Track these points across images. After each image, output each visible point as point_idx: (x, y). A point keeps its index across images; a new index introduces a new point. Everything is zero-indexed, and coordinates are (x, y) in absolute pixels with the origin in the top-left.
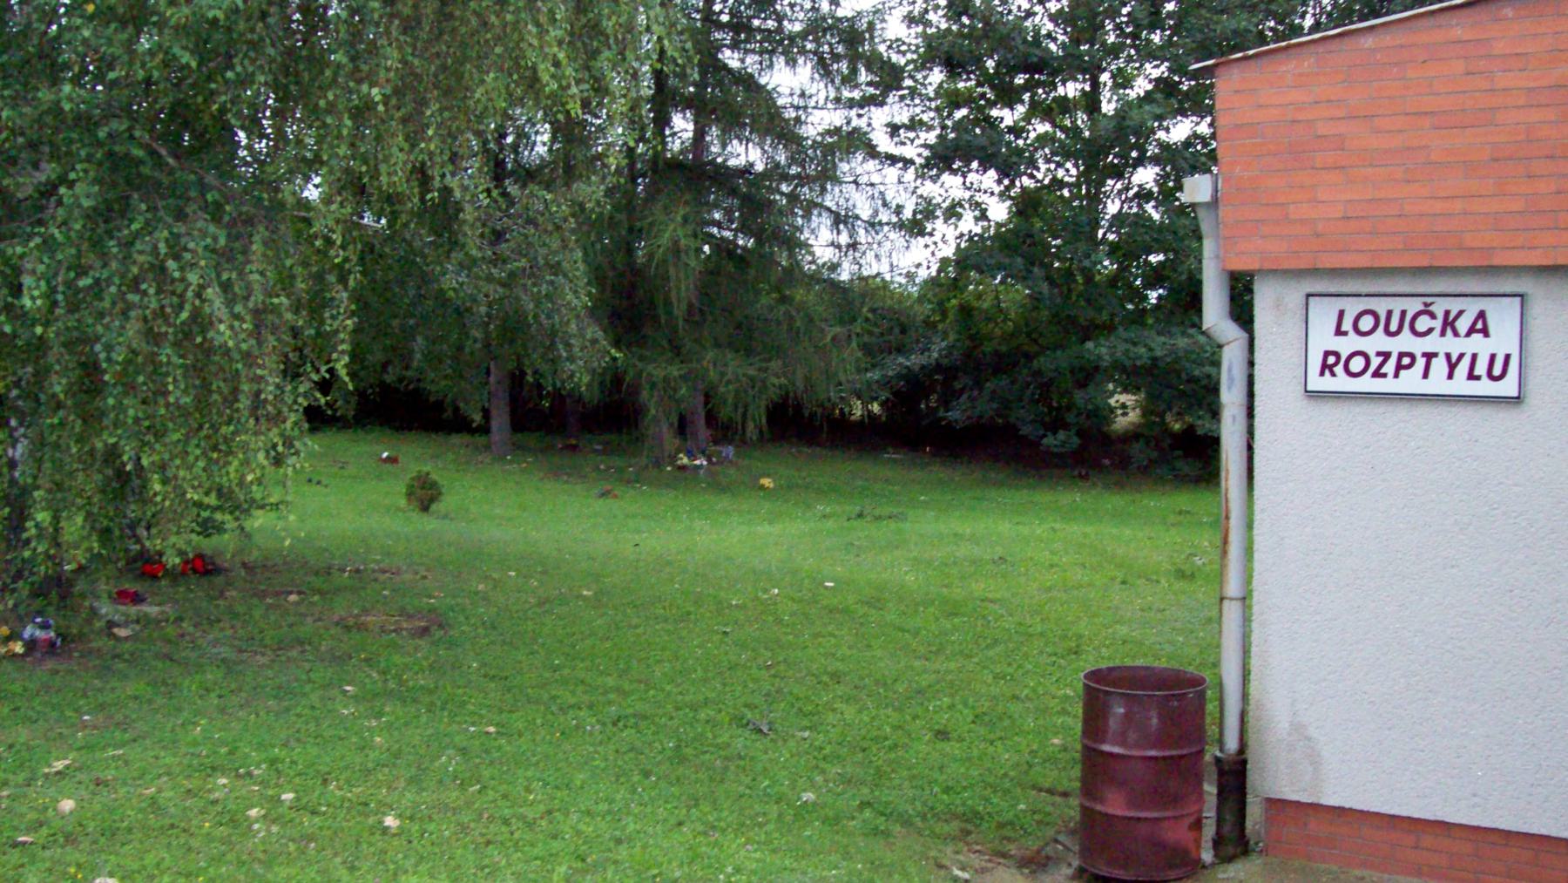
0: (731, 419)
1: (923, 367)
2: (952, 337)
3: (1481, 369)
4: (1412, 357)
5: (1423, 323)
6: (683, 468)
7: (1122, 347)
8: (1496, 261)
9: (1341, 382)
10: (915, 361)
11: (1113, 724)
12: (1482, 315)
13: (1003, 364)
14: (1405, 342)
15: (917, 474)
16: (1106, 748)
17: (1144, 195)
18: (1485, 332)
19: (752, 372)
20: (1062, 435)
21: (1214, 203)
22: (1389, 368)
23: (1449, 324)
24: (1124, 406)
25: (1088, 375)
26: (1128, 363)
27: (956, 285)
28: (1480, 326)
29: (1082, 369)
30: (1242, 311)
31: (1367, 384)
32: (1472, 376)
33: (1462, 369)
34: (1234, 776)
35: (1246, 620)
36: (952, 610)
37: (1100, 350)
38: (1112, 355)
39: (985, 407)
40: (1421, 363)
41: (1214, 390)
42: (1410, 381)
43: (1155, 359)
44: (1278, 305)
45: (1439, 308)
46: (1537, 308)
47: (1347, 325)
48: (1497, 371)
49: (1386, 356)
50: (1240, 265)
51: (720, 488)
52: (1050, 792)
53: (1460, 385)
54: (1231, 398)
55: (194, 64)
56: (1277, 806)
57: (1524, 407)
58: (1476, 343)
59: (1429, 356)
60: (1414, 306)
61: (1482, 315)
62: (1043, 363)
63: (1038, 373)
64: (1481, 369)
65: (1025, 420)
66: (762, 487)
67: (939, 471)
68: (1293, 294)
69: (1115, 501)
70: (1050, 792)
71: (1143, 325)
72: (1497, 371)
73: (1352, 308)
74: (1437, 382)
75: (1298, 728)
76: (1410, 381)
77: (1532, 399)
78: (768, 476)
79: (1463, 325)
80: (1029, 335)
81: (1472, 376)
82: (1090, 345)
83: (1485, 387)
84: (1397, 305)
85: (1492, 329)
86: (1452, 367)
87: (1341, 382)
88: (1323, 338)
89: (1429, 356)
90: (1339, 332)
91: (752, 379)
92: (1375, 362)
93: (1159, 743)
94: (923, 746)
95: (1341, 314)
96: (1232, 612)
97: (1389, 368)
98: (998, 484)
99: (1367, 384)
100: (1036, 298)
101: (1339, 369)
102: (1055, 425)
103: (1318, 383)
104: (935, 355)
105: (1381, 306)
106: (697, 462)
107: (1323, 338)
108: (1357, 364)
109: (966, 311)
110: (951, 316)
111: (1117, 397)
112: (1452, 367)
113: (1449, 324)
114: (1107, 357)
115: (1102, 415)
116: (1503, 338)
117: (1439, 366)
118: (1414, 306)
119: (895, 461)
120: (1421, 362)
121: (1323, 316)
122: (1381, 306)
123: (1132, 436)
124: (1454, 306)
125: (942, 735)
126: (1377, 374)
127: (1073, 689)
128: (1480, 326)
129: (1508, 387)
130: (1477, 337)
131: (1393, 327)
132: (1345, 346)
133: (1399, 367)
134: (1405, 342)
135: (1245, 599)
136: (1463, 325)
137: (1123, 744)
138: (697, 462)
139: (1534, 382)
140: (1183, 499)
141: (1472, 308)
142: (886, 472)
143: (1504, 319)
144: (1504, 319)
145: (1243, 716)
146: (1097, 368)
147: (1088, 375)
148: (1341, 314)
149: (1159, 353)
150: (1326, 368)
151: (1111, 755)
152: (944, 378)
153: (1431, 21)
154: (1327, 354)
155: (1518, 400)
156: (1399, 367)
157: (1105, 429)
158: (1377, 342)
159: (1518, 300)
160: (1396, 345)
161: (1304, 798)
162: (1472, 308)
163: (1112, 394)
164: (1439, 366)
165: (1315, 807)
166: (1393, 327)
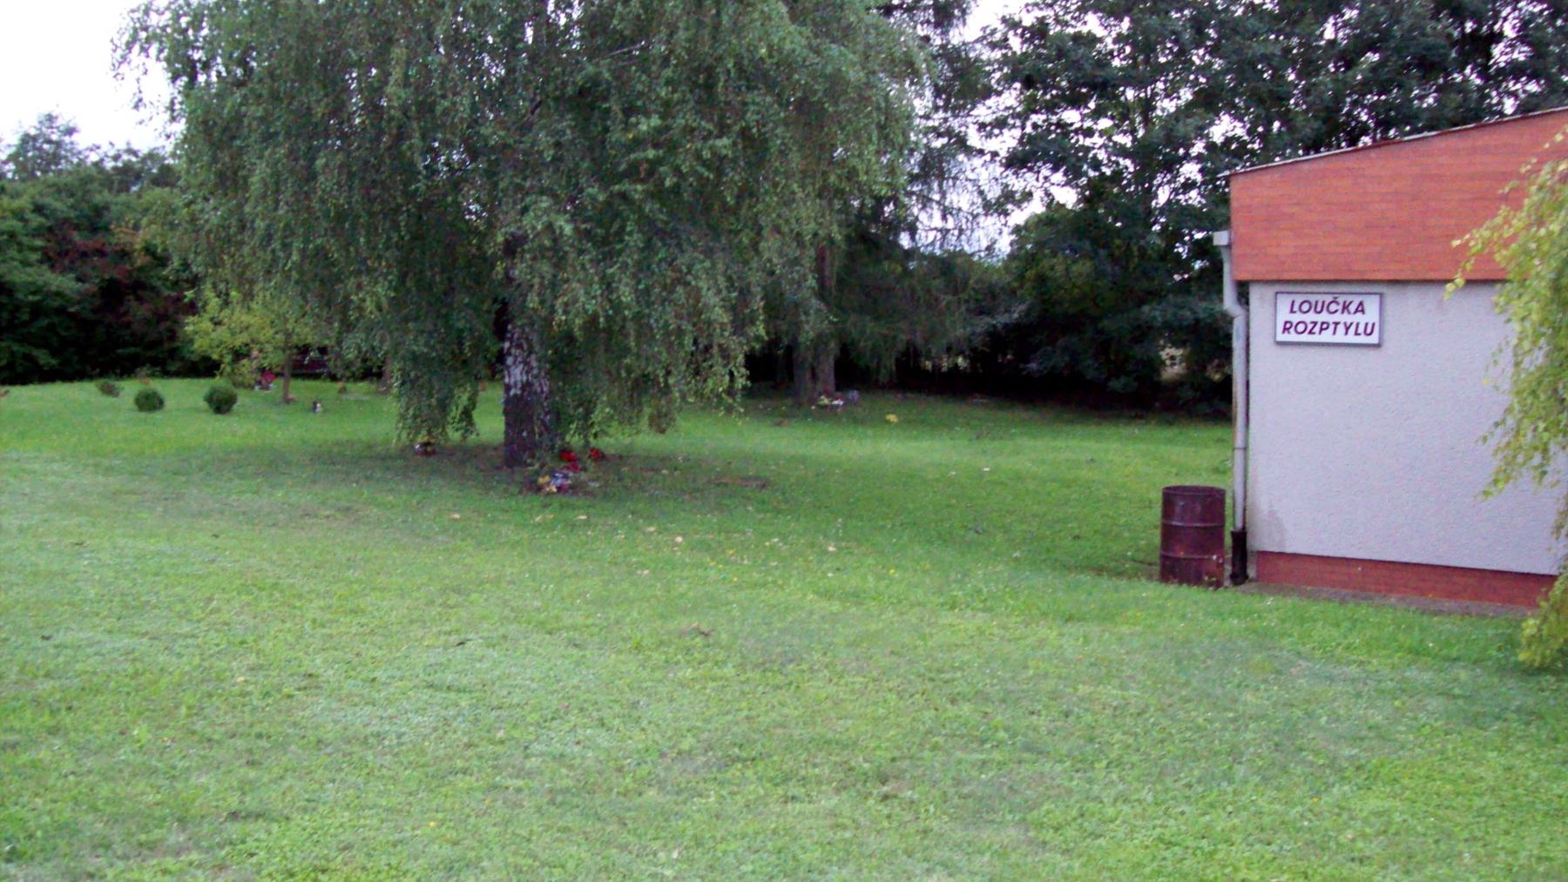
0: (868, 368)
1: (1006, 326)
2: (1029, 300)
3: (1361, 330)
4: (1328, 324)
5: (1333, 307)
6: (825, 407)
7: (1170, 311)
8: (1366, 277)
9: (1292, 337)
10: (1001, 319)
11: (1178, 510)
12: (1361, 304)
13: (1073, 324)
14: (1324, 317)
15: (1001, 414)
16: (1174, 523)
17: (1189, 185)
18: (1363, 311)
19: (885, 331)
20: (1123, 380)
21: (1229, 246)
22: (1317, 329)
23: (1345, 308)
24: (1173, 358)
25: (1144, 333)
26: (1176, 324)
27: (1032, 259)
28: (1361, 309)
29: (1139, 327)
30: (1243, 297)
31: (1305, 338)
32: (1357, 334)
33: (1352, 329)
34: (1240, 538)
35: (1246, 459)
36: (1067, 484)
37: (1153, 312)
38: (1164, 316)
39: (1059, 360)
40: (1332, 327)
41: (1229, 337)
42: (1327, 336)
43: (1197, 321)
44: (1261, 298)
45: (1341, 299)
46: (1388, 301)
47: (1296, 308)
48: (1369, 331)
49: (1315, 323)
50: (1244, 276)
51: (857, 421)
52: (1141, 562)
53: (1351, 338)
54: (1237, 344)
55: (711, 176)
56: (1264, 554)
57: (1383, 348)
58: (1359, 317)
59: (1336, 324)
60: (1328, 299)
61: (1361, 304)
62: (1106, 324)
63: (1101, 332)
64: (1361, 330)
65: (1090, 368)
66: (888, 422)
67: (1020, 413)
68: (1269, 292)
69: (1169, 432)
70: (1141, 562)
71: (1188, 292)
72: (1369, 331)
73: (1299, 299)
74: (1340, 337)
75: (1272, 513)
76: (1327, 336)
77: (1387, 344)
78: (893, 413)
79: (1352, 308)
80: (1094, 300)
81: (1357, 334)
82: (1146, 308)
83: (1362, 339)
84: (1320, 298)
85: (1366, 311)
86: (1347, 329)
87: (1292, 337)
88: (1284, 314)
89: (1336, 324)
90: (1292, 311)
91: (885, 337)
92: (1310, 327)
93: (1203, 520)
94: (1068, 542)
95: (1293, 303)
96: (1239, 455)
97: (1317, 329)
98: (1072, 422)
99: (1305, 338)
100: (1099, 274)
101: (1292, 330)
102: (1118, 371)
103: (1281, 337)
104: (1016, 315)
105: (1313, 298)
106: (836, 402)
107: (1284, 314)
108: (1301, 328)
109: (1042, 279)
110: (1028, 285)
111: (1168, 350)
112: (1347, 329)
113: (1345, 308)
114: (1160, 319)
115: (1155, 365)
116: (1371, 315)
117: (1341, 328)
118: (1328, 299)
119: (983, 404)
120: (1332, 327)
121: (1284, 304)
122: (1313, 298)
123: (1177, 384)
124: (1349, 298)
125: (1077, 538)
126: (1310, 332)
127: (1157, 497)
128: (1361, 309)
129: (1374, 339)
130: (1359, 314)
131: (1319, 309)
132: (1296, 318)
133: (1321, 329)
134: (1324, 317)
135: (1245, 449)
136: (1352, 308)
137: (1182, 520)
138: (836, 402)
139: (1386, 336)
140: (1218, 432)
141: (1356, 300)
142: (979, 412)
143: (1372, 305)
144: (1372, 305)
145: (1245, 510)
146: (1150, 328)
147: (1144, 333)
148: (1293, 303)
149: (1202, 315)
150: (1285, 330)
151: (1176, 527)
152: (1019, 338)
153: (1334, 159)
154: (1286, 323)
155: (1378, 346)
156: (1321, 329)
157: (1156, 379)
158: (1311, 317)
159: (1377, 297)
160: (1320, 318)
161: (1276, 549)
162: (1356, 300)
163: (1163, 348)
164: (1341, 328)
165: (1281, 554)
166: (1319, 309)
